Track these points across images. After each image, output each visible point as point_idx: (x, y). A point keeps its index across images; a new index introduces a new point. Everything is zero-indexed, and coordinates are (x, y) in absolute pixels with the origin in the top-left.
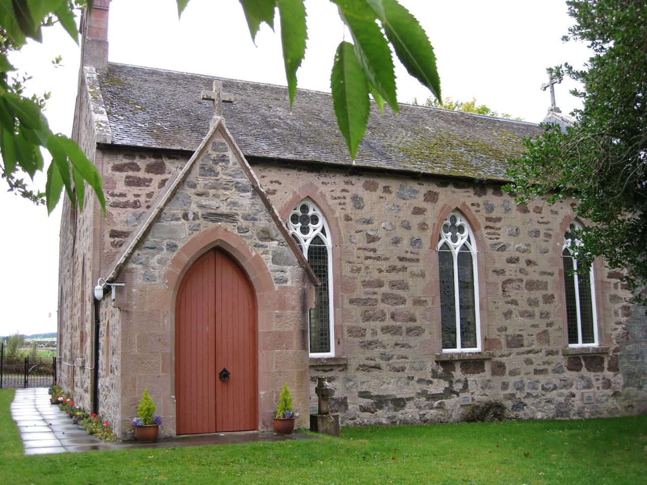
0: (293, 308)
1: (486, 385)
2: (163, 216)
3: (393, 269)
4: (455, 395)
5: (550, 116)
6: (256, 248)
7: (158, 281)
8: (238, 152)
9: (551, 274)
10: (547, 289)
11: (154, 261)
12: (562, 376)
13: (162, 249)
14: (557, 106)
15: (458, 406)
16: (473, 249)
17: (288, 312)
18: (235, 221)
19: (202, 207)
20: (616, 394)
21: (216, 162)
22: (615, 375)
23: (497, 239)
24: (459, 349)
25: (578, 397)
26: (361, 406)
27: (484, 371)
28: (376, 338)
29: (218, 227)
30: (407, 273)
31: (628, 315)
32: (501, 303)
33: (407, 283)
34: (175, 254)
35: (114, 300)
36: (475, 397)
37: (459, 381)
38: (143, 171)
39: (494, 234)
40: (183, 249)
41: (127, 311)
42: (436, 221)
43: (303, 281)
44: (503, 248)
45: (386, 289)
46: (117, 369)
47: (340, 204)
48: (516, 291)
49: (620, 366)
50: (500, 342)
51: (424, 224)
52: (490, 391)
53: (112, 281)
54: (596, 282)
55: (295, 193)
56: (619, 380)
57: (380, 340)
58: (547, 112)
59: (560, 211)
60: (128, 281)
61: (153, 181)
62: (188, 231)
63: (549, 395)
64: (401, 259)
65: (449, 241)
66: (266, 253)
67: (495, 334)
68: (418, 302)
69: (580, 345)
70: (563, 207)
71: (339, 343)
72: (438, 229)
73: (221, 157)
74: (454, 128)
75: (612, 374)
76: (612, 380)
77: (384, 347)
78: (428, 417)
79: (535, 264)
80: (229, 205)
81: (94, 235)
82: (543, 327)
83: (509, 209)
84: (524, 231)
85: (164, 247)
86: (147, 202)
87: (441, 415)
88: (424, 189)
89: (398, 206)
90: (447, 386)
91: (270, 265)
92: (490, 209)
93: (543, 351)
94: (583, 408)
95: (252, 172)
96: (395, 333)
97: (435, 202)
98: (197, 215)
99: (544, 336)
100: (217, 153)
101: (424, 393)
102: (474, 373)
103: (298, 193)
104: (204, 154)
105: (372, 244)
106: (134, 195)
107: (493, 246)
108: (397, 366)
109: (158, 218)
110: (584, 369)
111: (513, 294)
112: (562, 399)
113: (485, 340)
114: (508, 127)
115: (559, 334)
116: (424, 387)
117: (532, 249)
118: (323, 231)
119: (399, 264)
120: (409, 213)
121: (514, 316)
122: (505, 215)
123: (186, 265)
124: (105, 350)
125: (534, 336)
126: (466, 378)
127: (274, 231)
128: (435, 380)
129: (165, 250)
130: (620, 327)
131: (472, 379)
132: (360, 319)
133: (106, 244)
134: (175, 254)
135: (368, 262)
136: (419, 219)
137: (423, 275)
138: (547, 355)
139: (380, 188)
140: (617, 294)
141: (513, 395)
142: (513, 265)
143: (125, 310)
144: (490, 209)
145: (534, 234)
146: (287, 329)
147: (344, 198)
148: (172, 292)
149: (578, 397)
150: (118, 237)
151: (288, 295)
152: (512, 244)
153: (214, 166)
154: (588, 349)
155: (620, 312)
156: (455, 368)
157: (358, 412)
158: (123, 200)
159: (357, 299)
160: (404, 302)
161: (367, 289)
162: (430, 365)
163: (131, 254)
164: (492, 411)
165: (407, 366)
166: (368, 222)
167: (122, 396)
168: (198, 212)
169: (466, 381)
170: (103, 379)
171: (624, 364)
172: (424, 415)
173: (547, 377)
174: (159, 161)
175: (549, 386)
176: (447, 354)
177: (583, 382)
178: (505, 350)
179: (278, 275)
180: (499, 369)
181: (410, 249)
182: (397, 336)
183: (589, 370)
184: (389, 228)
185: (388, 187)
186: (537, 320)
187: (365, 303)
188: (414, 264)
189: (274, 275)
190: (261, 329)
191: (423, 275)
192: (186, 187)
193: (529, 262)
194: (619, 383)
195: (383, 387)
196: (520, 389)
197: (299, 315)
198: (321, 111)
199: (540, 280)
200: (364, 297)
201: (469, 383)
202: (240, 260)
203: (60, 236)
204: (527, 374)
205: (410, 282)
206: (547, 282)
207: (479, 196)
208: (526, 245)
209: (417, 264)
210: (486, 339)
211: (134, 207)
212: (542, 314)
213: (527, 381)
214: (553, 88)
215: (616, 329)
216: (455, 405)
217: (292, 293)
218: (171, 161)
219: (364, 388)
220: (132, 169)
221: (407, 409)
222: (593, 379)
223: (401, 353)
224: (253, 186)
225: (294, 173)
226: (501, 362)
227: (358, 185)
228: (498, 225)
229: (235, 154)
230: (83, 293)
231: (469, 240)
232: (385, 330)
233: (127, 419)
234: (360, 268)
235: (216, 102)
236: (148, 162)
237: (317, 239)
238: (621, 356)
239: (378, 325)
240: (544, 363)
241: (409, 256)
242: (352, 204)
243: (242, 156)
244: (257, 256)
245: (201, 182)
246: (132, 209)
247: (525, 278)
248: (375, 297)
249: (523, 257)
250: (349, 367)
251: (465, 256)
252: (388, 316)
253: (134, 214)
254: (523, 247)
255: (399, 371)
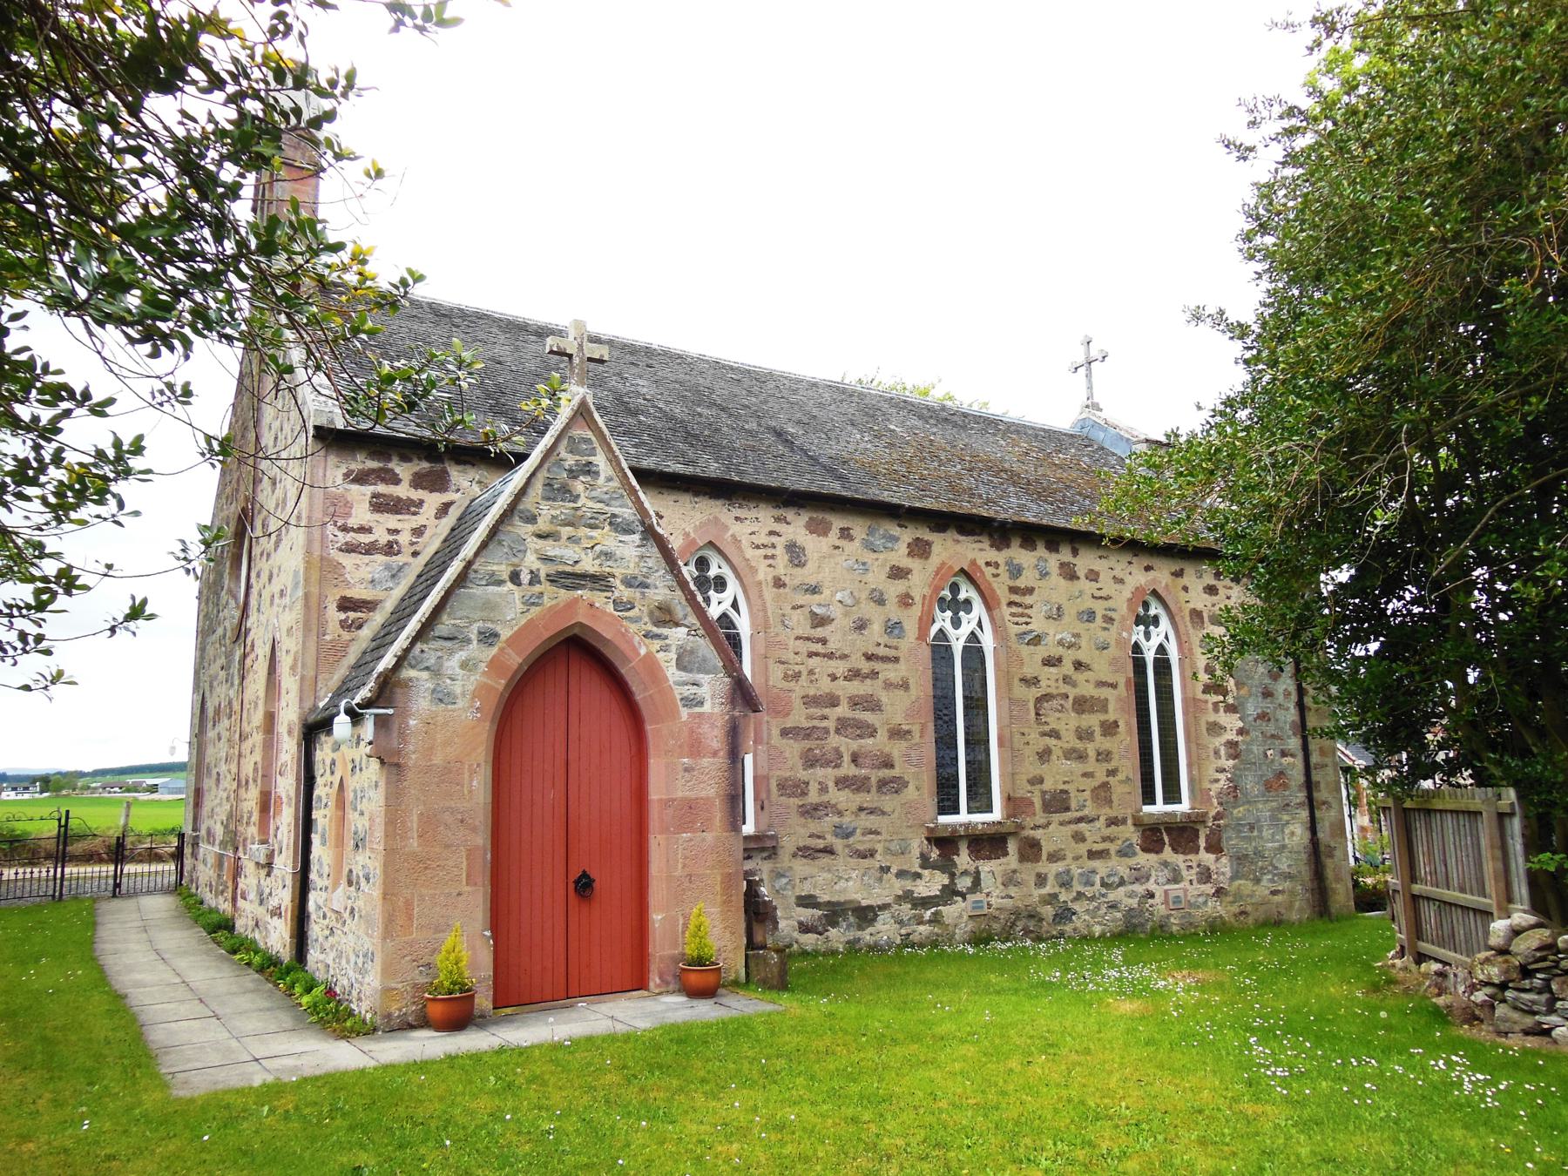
0: (715, 754)
1: (1010, 880)
2: (472, 575)
3: (855, 674)
4: (959, 899)
5: (1084, 416)
6: (647, 641)
7: (461, 704)
8: (616, 457)
9: (1114, 686)
10: (1106, 712)
11: (453, 664)
12: (1132, 862)
13: (469, 641)
14: (1095, 400)
15: (965, 917)
16: (988, 641)
17: (706, 761)
18: (609, 588)
19: (546, 559)
20: (1219, 892)
21: (573, 474)
22: (1217, 859)
23: (1027, 623)
24: (963, 817)
25: (1159, 898)
26: (801, 924)
27: (1006, 854)
28: (825, 798)
29: (576, 600)
30: (879, 682)
31: (1235, 757)
32: (1033, 736)
33: (879, 700)
34: (494, 650)
35: (370, 743)
36: (993, 901)
37: (965, 873)
38: (405, 484)
39: (1022, 615)
40: (511, 641)
41: (398, 765)
42: (927, 591)
43: (732, 702)
44: (1037, 640)
45: (842, 710)
46: (368, 879)
47: (766, 557)
48: (1057, 715)
49: (1224, 844)
50: (1032, 804)
51: (908, 596)
52: (1016, 889)
53: (368, 704)
54: (1185, 700)
55: (687, 535)
56: (1223, 867)
57: (833, 802)
58: (1079, 410)
59: (1128, 579)
60: (401, 705)
61: (426, 505)
62: (519, 607)
63: (1112, 896)
64: (869, 657)
65: (948, 626)
66: (665, 649)
67: (1023, 790)
68: (897, 733)
69: (1159, 807)
70: (1134, 571)
71: (762, 808)
72: (931, 610)
73: (585, 465)
74: (935, 430)
75: (1212, 857)
76: (1213, 867)
77: (840, 814)
78: (915, 938)
79: (1088, 668)
80: (598, 557)
81: (307, 606)
82: (1101, 777)
83: (1047, 574)
84: (1070, 611)
85: (474, 636)
86: (412, 544)
87: (938, 935)
88: (907, 535)
89: (864, 564)
90: (946, 882)
91: (672, 673)
92: (1016, 571)
93: (1102, 819)
94: (1168, 916)
95: (641, 494)
96: (858, 790)
97: (927, 558)
98: (537, 576)
99: (1102, 793)
100: (578, 458)
101: (907, 896)
102: (990, 858)
103: (692, 535)
104: (553, 459)
105: (819, 629)
106: (389, 530)
107: (1021, 636)
108: (861, 847)
109: (462, 579)
110: (1167, 849)
111: (1053, 719)
112: (1134, 902)
113: (1009, 799)
114: (1018, 432)
115: (1127, 789)
116: (908, 884)
117: (1084, 643)
118: (735, 605)
119: (866, 667)
120: (883, 576)
121: (1054, 757)
122: (1040, 583)
123: (516, 671)
124: (331, 835)
125: (1087, 793)
126: (977, 868)
127: (681, 608)
128: (926, 873)
129: (475, 642)
130: (1222, 776)
131: (987, 869)
132: (800, 763)
133: (330, 624)
134: (494, 650)
135: (814, 661)
136: (899, 587)
137: (905, 686)
138: (1108, 826)
139: (834, 532)
140: (1218, 720)
141: (1055, 896)
142: (1052, 669)
143: (390, 762)
144: (1016, 571)
145: (1085, 617)
146: (703, 794)
147: (773, 546)
148: (488, 724)
149: (1159, 898)
150: (355, 611)
151: (706, 728)
152: (1051, 632)
153: (570, 482)
154: (1173, 814)
155: (1223, 752)
156: (958, 849)
157: (796, 934)
158: (365, 539)
159: (795, 728)
160: (873, 733)
161: (812, 711)
162: (917, 844)
163: (407, 651)
164: (1020, 925)
165: (879, 847)
166: (814, 590)
167: (384, 939)
168: (538, 570)
169: (978, 873)
170: (324, 894)
171: (1231, 841)
172: (909, 934)
173: (1110, 864)
174: (438, 467)
175: (1112, 879)
176: (946, 826)
177: (1166, 871)
178: (1040, 818)
179: (688, 691)
180: (1031, 850)
181: (884, 639)
182: (862, 794)
183: (1175, 850)
184: (849, 602)
185: (848, 529)
186: (1091, 765)
187: (808, 736)
188: (890, 666)
189: (680, 692)
190: (656, 793)
191: (905, 686)
192: (517, 521)
193: (1078, 665)
194: (1223, 874)
195: (837, 887)
196: (1066, 884)
197: (725, 767)
198: (712, 391)
199: (1096, 696)
200: (806, 724)
201: (982, 877)
202: (617, 663)
203: (199, 598)
204: (1076, 858)
205: (884, 697)
206: (1107, 700)
207: (999, 549)
208: (1074, 636)
209: (896, 666)
210: (1009, 798)
211: (386, 554)
212: (1099, 754)
213: (1076, 871)
214: (1089, 370)
215: (1217, 781)
216: (960, 916)
217: (713, 726)
218: (461, 468)
219: (806, 889)
220: (384, 480)
221: (879, 926)
222: (1183, 866)
223: (868, 825)
224: (643, 523)
225: (686, 499)
226: (1033, 839)
227: (796, 526)
228: (1028, 600)
229: (610, 461)
230: (270, 719)
231: (980, 624)
232: (842, 783)
233: (393, 985)
234: (800, 672)
235: (576, 360)
236: (417, 469)
237: (723, 619)
238: (1226, 826)
239: (828, 774)
240: (1104, 839)
241: (882, 651)
242: (786, 557)
243: (625, 465)
244: (649, 655)
245: (547, 512)
246: (384, 558)
247: (1073, 693)
248: (825, 724)
249: (1069, 656)
250: (781, 852)
251: (974, 653)
252: (847, 758)
253: (388, 567)
254: (1069, 638)
255: (865, 857)
